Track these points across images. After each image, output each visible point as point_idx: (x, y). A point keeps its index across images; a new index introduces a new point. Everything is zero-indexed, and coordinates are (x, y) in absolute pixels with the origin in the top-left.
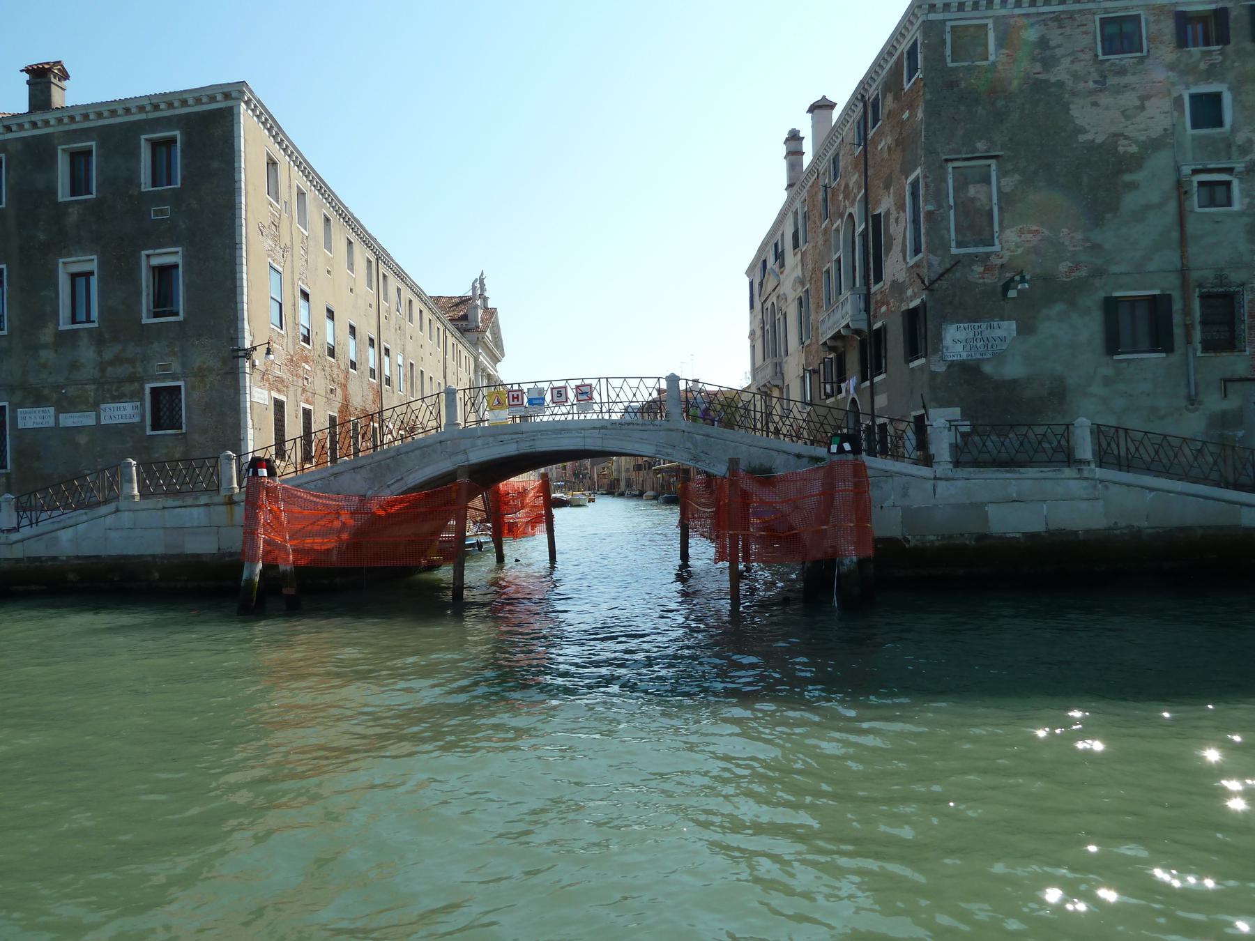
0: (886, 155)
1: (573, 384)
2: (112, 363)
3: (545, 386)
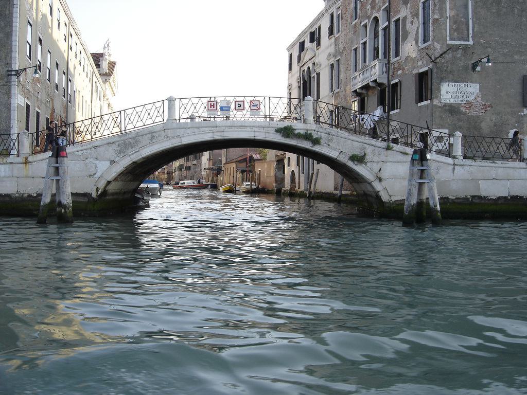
1: (248, 99)
3: (231, 99)
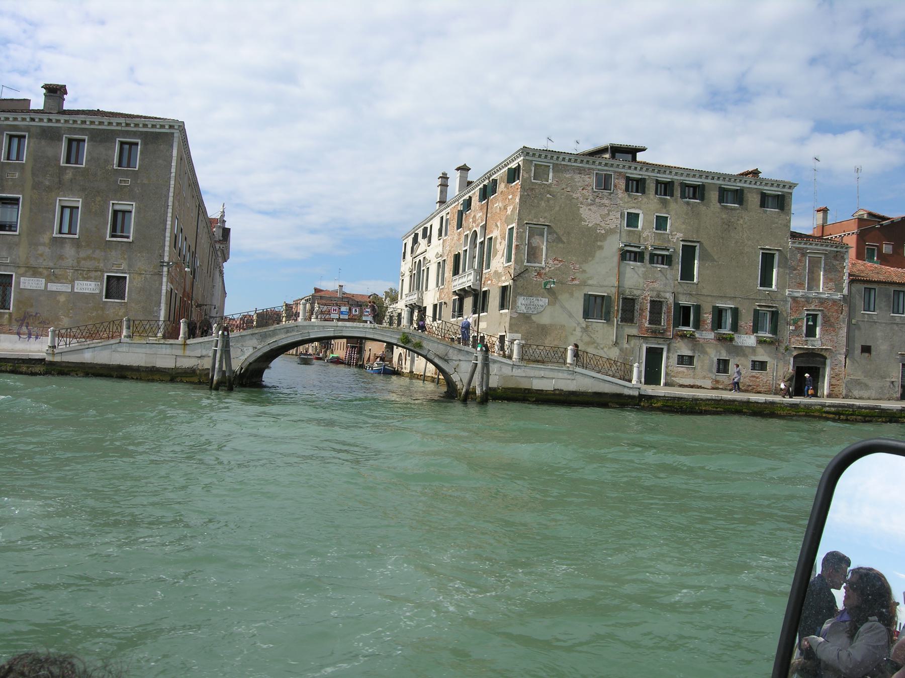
0: (498, 210)
2: (85, 259)
